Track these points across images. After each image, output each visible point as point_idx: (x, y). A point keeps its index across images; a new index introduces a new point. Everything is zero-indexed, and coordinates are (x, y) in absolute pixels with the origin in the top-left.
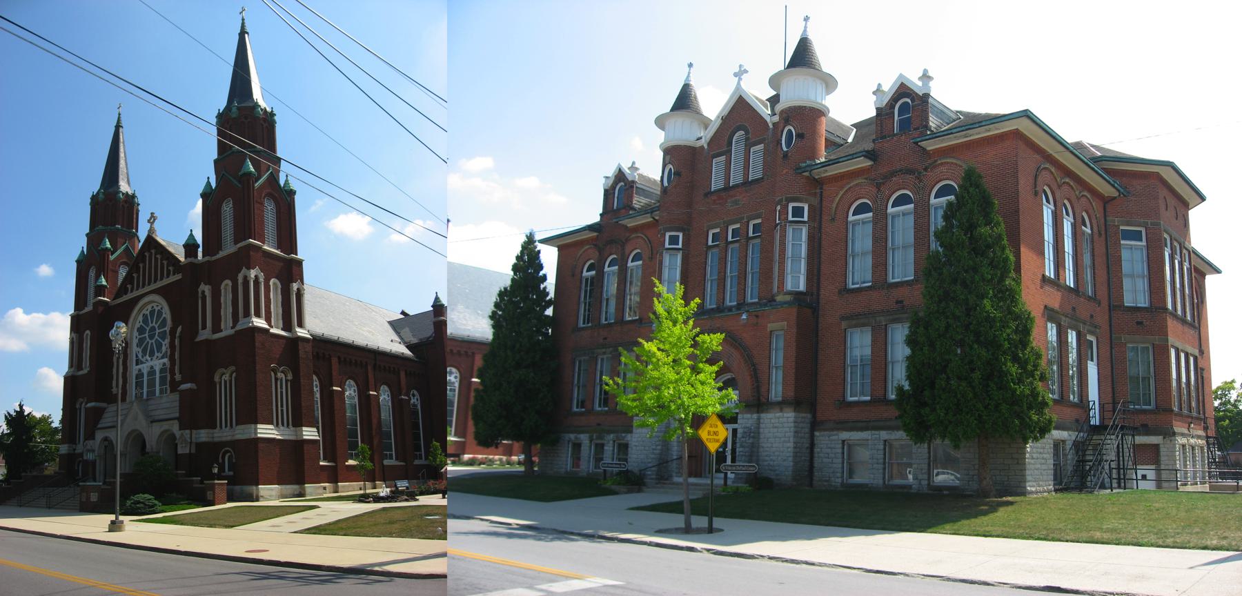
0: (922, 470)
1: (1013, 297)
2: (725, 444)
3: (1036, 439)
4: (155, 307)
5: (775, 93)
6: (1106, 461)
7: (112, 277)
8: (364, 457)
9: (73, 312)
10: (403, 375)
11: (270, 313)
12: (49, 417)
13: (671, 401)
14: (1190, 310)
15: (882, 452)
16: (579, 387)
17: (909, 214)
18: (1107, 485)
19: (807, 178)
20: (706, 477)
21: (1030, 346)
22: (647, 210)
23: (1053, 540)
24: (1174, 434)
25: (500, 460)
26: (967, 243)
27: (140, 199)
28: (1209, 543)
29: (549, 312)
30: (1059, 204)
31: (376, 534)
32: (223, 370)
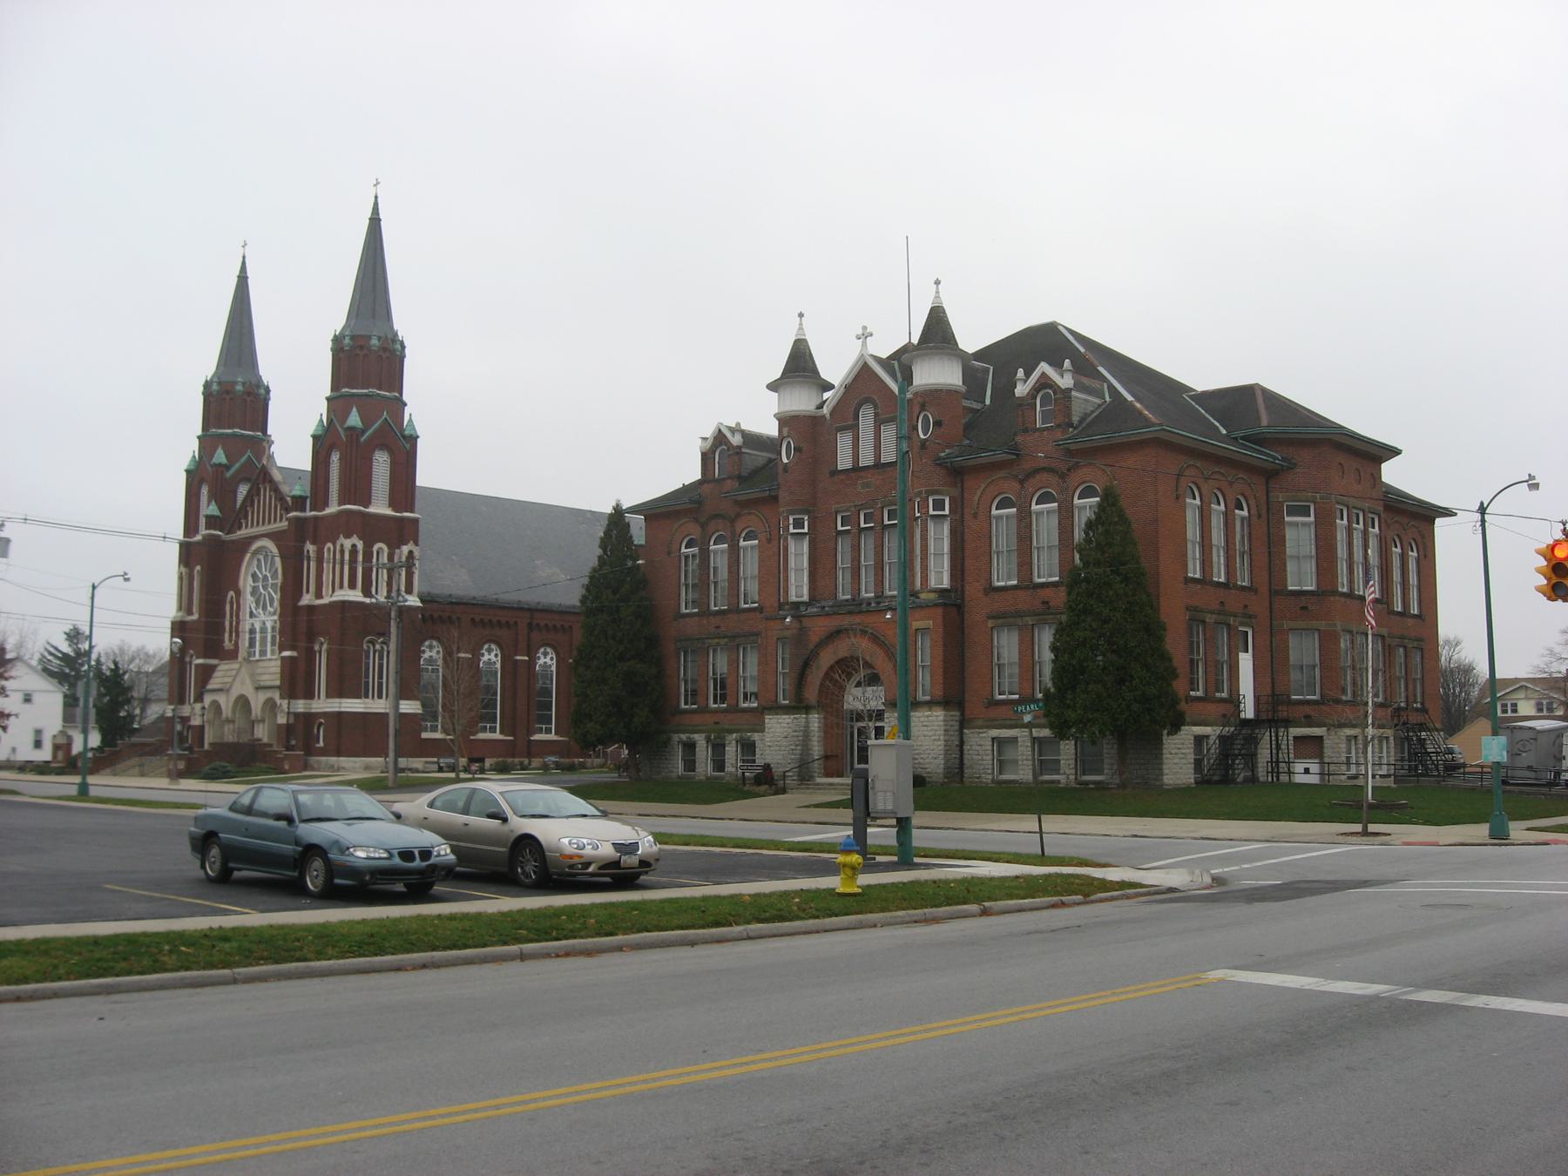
17: (1053, 511)
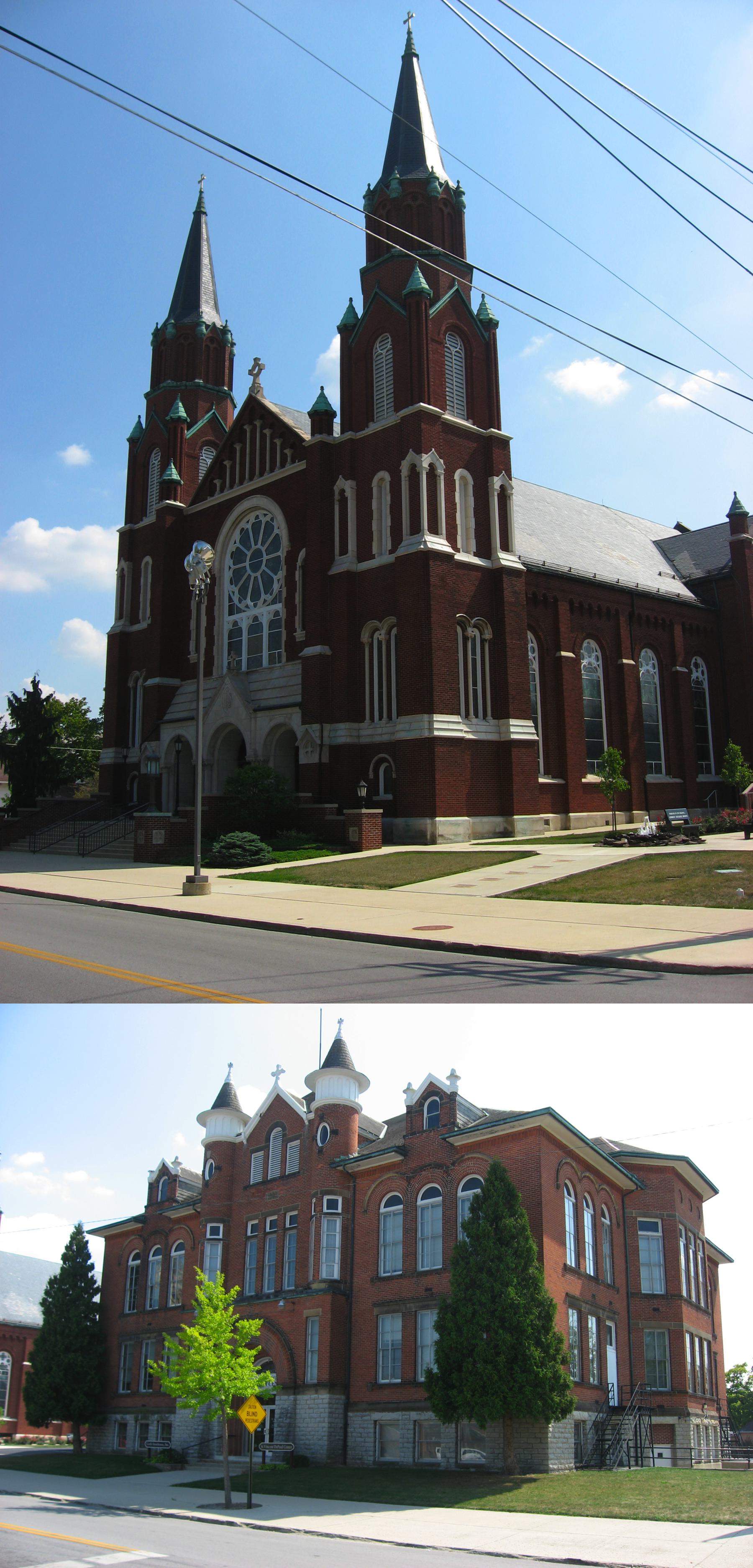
0: (449, 1448)
1: (537, 1285)
2: (263, 1424)
3: (557, 1419)
4: (261, 518)
5: (309, 1091)
6: (624, 1440)
7: (188, 465)
8: (614, 771)
9: (123, 525)
10: (678, 631)
11: (455, 527)
12: (83, 702)
13: (212, 1383)
14: (704, 1296)
15: (412, 1432)
16: (125, 1370)
17: (437, 1206)
18: (625, 1463)
19: (341, 1172)
20: (245, 1455)
21: (553, 1331)
22: (190, 1202)
23: (574, 1515)
24: (689, 1414)
25: (51, 1439)
26: (493, 1234)
27: (237, 335)
28: (721, 1518)
29: (97, 1299)
30: (579, 1197)
31: (633, 900)
32: (376, 623)
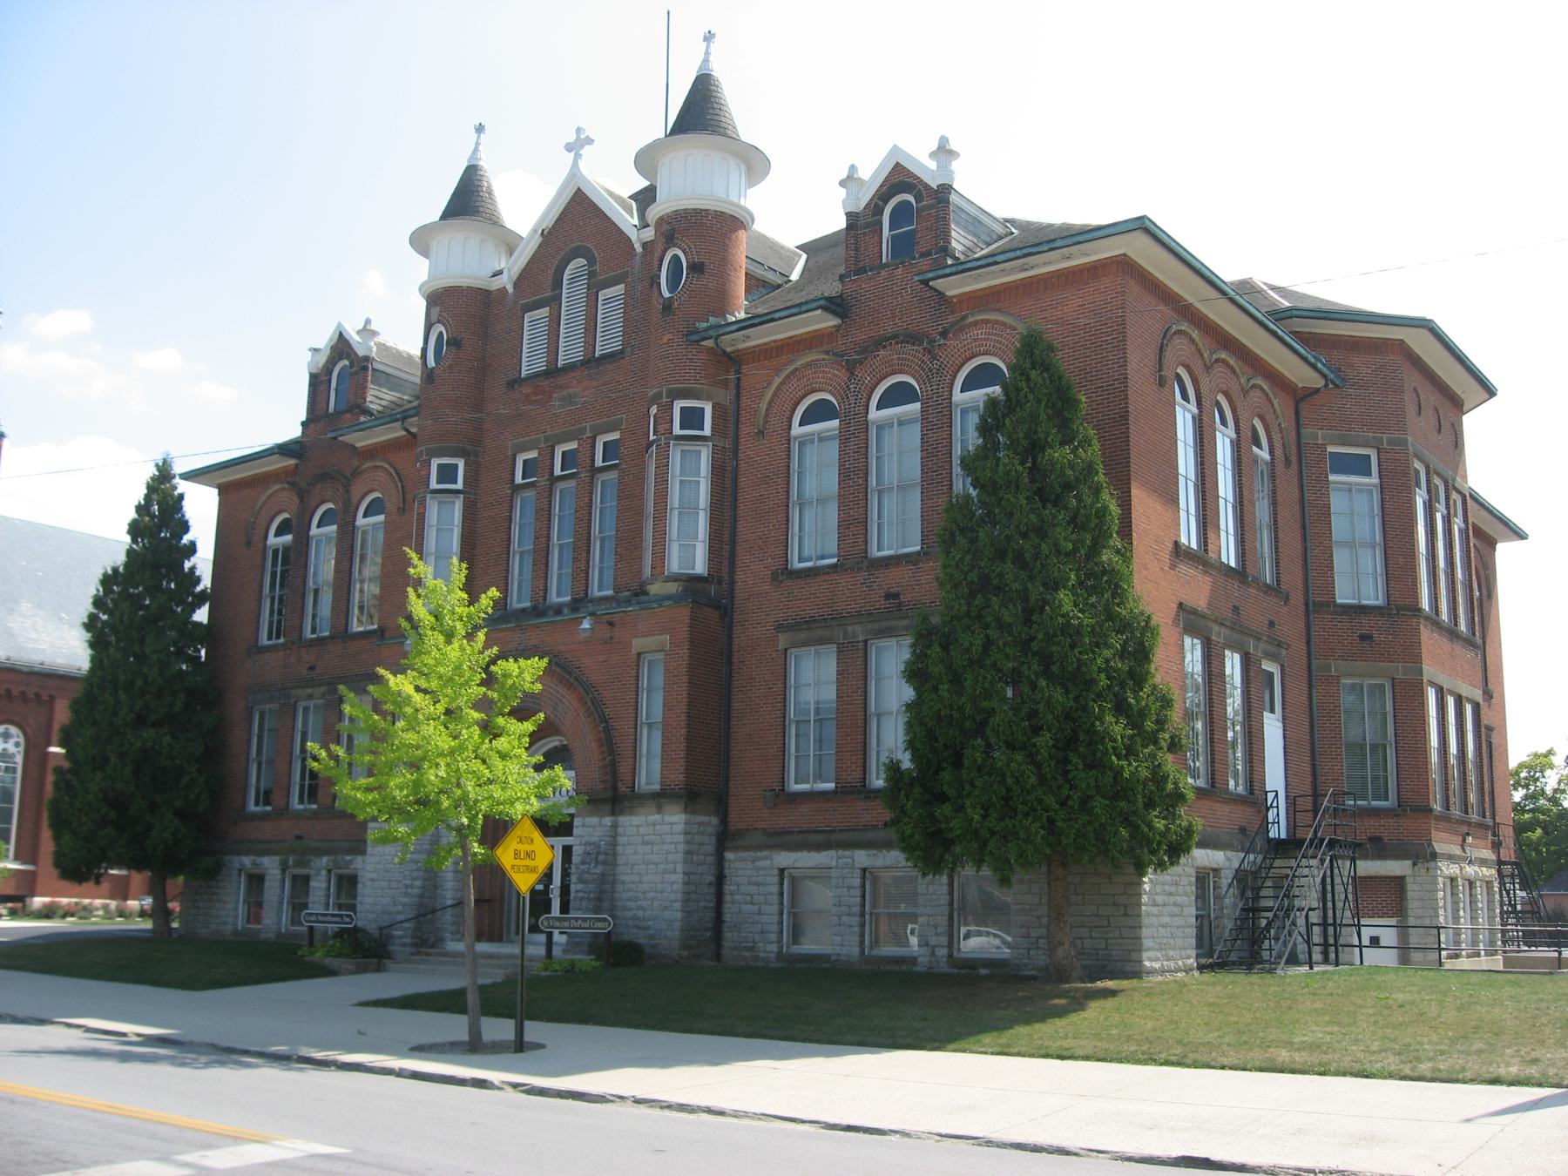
17: (911, 421)
